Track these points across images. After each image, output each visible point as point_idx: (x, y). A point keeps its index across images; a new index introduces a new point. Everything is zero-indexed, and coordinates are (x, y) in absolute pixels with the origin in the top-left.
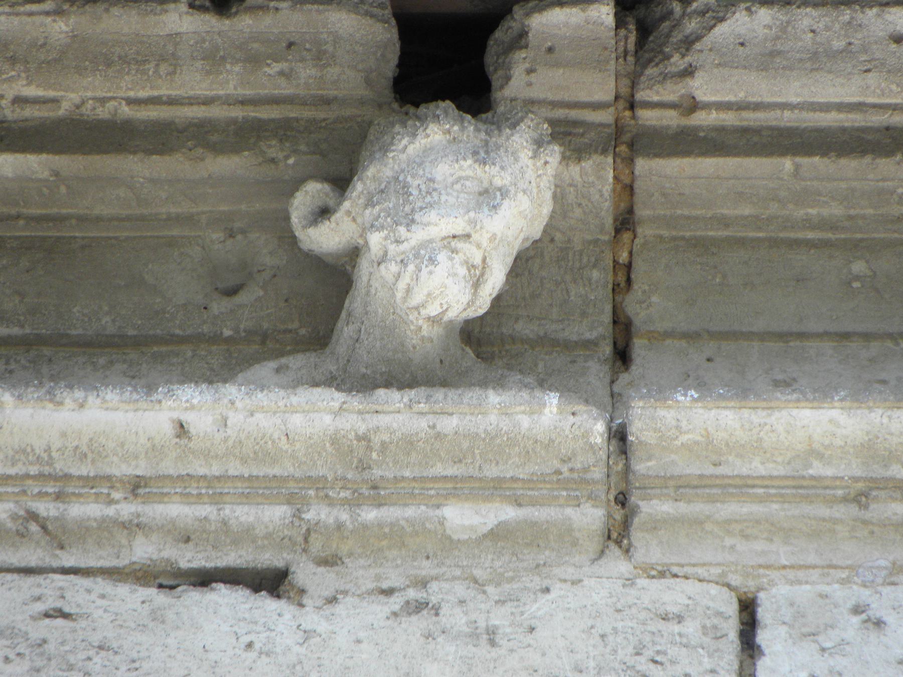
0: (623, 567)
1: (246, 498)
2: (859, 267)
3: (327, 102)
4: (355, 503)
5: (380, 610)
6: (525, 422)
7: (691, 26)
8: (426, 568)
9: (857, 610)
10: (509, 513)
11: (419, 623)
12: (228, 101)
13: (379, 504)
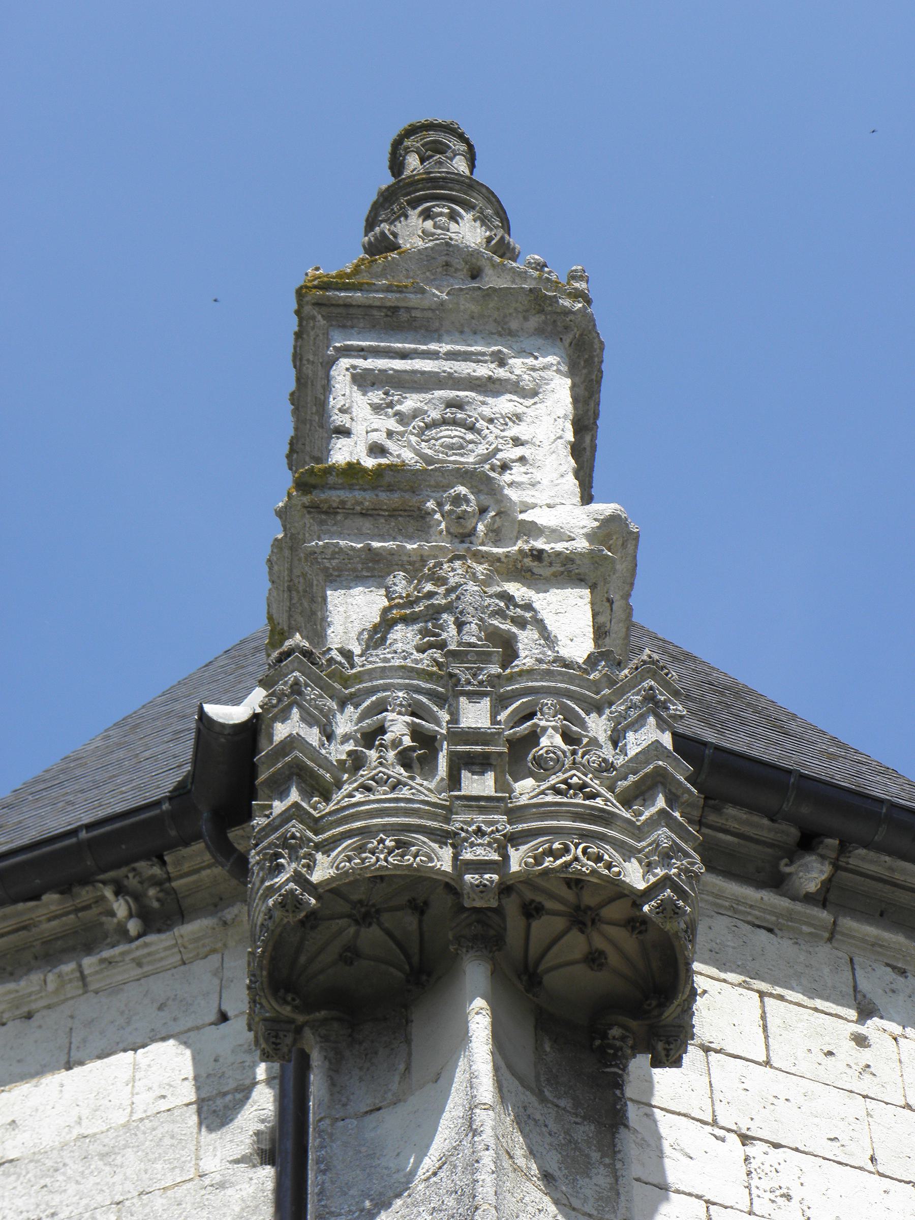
0: (830, 946)
1: (769, 914)
2: (868, 901)
3: (787, 844)
4: (787, 921)
5: (790, 942)
6: (820, 915)
7: (851, 849)
8: (797, 936)
9: (870, 966)
10: (813, 930)
11: (796, 946)
12: (770, 838)
13: (792, 922)
